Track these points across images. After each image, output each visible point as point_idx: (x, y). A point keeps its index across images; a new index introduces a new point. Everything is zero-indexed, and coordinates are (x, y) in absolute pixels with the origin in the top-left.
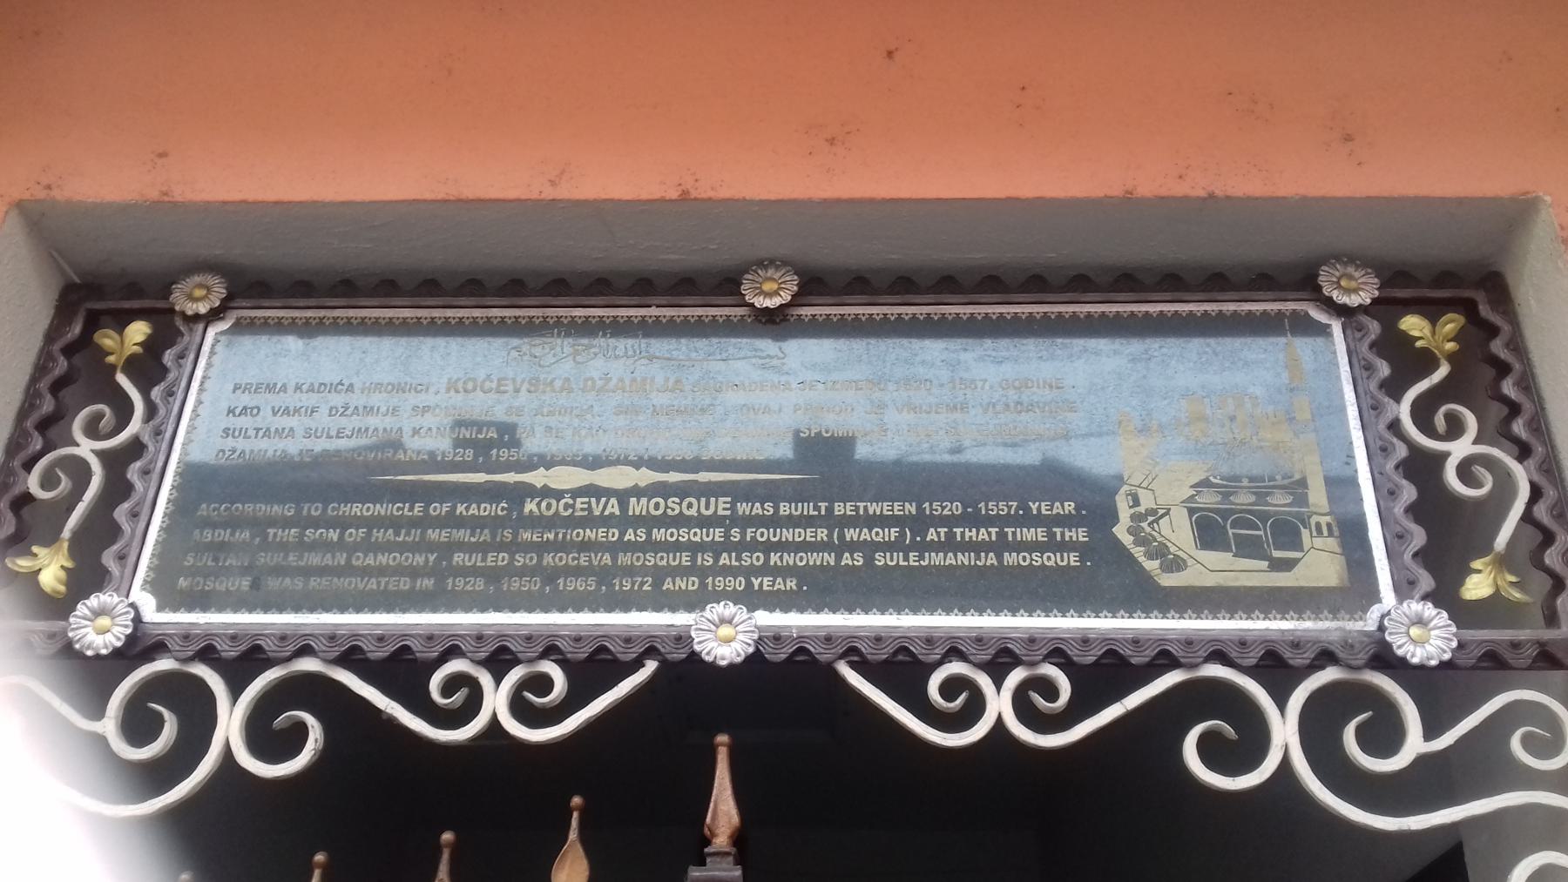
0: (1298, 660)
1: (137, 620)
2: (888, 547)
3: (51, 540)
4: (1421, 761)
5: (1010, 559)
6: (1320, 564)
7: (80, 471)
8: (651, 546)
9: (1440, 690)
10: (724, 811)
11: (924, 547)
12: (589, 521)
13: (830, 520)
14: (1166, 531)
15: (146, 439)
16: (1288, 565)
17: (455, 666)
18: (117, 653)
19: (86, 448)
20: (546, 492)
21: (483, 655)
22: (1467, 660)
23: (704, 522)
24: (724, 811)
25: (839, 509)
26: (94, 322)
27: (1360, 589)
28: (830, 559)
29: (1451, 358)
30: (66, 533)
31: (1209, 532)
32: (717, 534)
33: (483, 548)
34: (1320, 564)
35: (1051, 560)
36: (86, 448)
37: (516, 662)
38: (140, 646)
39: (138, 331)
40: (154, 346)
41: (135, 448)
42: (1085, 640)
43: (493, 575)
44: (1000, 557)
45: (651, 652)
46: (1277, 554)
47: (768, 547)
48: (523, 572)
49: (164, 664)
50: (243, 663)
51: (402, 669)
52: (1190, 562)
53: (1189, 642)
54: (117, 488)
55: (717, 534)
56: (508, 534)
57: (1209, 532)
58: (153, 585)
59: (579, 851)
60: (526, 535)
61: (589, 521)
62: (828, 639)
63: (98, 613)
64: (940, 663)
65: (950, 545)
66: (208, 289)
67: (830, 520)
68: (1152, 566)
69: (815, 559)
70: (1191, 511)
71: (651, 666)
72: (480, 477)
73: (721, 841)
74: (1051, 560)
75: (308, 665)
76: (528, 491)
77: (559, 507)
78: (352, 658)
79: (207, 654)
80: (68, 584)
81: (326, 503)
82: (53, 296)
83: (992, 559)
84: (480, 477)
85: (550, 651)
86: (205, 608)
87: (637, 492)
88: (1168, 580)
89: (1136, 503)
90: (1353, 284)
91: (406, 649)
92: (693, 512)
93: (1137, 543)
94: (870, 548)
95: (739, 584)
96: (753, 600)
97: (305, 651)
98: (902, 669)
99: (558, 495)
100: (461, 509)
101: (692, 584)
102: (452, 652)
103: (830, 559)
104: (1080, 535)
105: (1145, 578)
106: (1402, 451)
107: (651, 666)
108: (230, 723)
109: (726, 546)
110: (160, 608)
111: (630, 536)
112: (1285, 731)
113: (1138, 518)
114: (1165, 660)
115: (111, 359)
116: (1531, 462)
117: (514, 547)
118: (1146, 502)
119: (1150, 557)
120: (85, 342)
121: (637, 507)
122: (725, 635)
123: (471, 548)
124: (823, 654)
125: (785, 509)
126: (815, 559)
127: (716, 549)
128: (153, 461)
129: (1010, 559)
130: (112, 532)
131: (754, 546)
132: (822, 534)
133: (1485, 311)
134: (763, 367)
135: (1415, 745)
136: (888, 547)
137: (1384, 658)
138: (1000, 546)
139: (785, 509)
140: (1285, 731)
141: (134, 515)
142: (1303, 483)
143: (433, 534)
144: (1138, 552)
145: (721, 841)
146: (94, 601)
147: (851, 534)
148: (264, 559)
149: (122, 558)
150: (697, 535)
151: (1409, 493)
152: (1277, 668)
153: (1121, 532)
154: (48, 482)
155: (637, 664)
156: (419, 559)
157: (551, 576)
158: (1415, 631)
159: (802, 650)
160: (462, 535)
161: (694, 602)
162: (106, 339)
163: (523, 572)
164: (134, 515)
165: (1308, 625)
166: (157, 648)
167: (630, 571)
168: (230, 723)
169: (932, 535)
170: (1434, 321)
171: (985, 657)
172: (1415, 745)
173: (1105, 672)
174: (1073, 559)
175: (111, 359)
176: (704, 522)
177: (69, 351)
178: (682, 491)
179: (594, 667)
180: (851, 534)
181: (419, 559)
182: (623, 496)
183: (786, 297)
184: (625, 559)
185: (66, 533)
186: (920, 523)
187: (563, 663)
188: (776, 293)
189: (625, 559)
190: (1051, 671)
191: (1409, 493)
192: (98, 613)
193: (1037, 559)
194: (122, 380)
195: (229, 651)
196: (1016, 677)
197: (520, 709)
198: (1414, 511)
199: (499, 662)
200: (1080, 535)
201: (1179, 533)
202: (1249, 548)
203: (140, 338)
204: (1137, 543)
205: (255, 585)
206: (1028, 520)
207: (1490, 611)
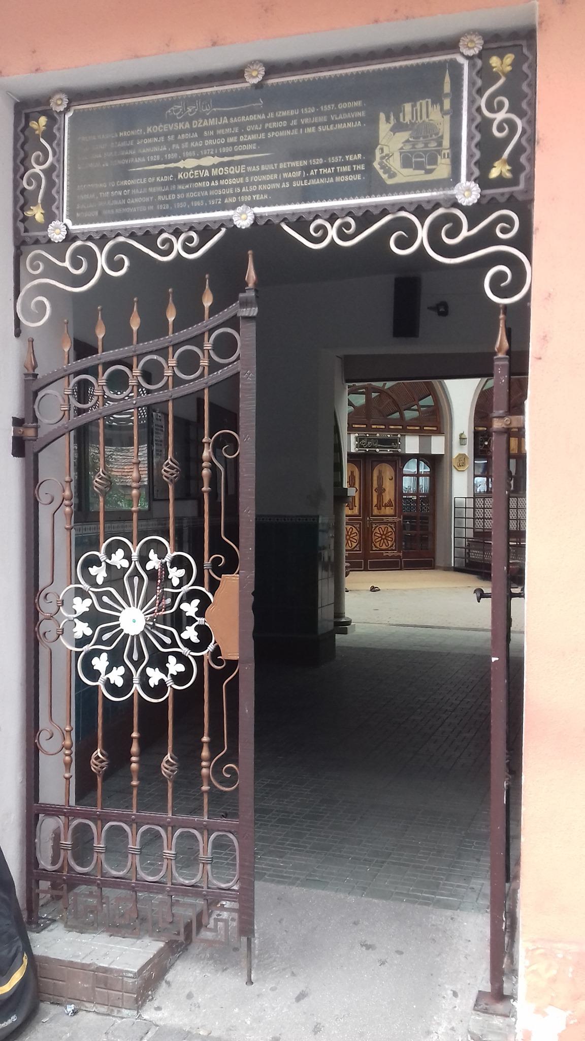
0: (428, 207)
1: (67, 229)
3: (35, 204)
4: (466, 240)
5: (338, 179)
6: (442, 170)
8: (220, 187)
9: (475, 213)
10: (251, 275)
11: (308, 178)
12: (200, 180)
13: (279, 171)
14: (391, 163)
15: (477, 97)
16: (429, 172)
17: (319, 221)
18: (64, 241)
19: (38, 169)
22: (484, 201)
23: (237, 176)
24: (251, 275)
25: (281, 165)
26: (28, 118)
27: (455, 178)
28: (278, 185)
29: (506, 75)
30: (39, 201)
32: (241, 180)
33: (167, 193)
34: (442, 170)
35: (351, 178)
36: (38, 169)
38: (70, 238)
39: (43, 120)
41: (52, 168)
42: (359, 208)
44: (334, 179)
45: (222, 225)
46: (428, 167)
47: (258, 183)
48: (180, 201)
49: (79, 243)
50: (102, 239)
51: (148, 237)
53: (393, 204)
54: (51, 184)
55: (241, 180)
56: (174, 187)
57: (406, 162)
59: (209, 292)
60: (180, 187)
61: (200, 180)
62: (277, 216)
63: (56, 228)
64: (314, 220)
65: (319, 176)
66: (62, 100)
67: (279, 171)
68: (385, 176)
69: (274, 186)
70: (401, 153)
71: (223, 230)
72: (162, 166)
73: (251, 285)
74: (351, 178)
75: (121, 239)
76: (178, 170)
77: (189, 175)
78: (132, 236)
79: (90, 238)
80: (45, 218)
81: (116, 181)
83: (332, 180)
84: (162, 166)
86: (127, 219)
87: (215, 166)
88: (389, 182)
89: (382, 152)
90: (473, 45)
91: (207, 226)
92: (233, 172)
93: (381, 168)
94: (291, 180)
95: (249, 198)
96: (252, 204)
97: (118, 235)
98: (301, 223)
99: (188, 170)
101: (234, 200)
102: (317, 217)
103: (278, 185)
104: (362, 167)
105: (382, 181)
106: (479, 119)
107: (223, 230)
108: (102, 261)
110: (73, 224)
111: (213, 184)
112: (422, 234)
113: (382, 158)
114: (384, 212)
115: (37, 132)
116: (525, 119)
117: (176, 192)
118: (386, 151)
119: (385, 173)
121: (215, 172)
122: (243, 219)
125: (263, 168)
126: (274, 186)
127: (240, 186)
128: (59, 172)
130: (53, 200)
131: (253, 183)
132: (276, 176)
133: (525, 51)
135: (465, 233)
137: (456, 205)
138: (336, 174)
139: (263, 168)
140: (422, 234)
141: (58, 192)
142: (442, 137)
143: (151, 190)
144: (381, 172)
145: (251, 285)
146: (53, 224)
147: (285, 175)
148: (101, 204)
149: (58, 208)
151: (478, 137)
152: (421, 211)
153: (376, 165)
154: (29, 184)
155: (219, 230)
156: (147, 199)
157: (189, 201)
158: (466, 194)
159: (367, 211)
161: (234, 207)
163: (180, 201)
164: (58, 192)
165: (435, 194)
167: (214, 197)
168: (102, 261)
169: (312, 173)
170: (502, 57)
171: (412, 209)
172: (465, 233)
173: (366, 218)
174: (359, 177)
175: (37, 132)
176: (237, 176)
177: (23, 131)
178: (229, 164)
179: (206, 232)
180: (285, 175)
181: (147, 199)
182: (209, 168)
183: (260, 78)
184: (212, 193)
185: (39, 201)
186: (307, 169)
187: (354, 218)
188: (257, 76)
189: (212, 193)
190: (350, 220)
191: (478, 137)
192: (56, 228)
193: (347, 178)
195: (140, 233)
196: (338, 223)
197: (342, 236)
198: (477, 145)
199: (177, 233)
200: (362, 167)
201: (395, 163)
202: (419, 166)
203: (44, 124)
204: (381, 168)
205: (100, 213)
206: (346, 163)
207: (501, 181)
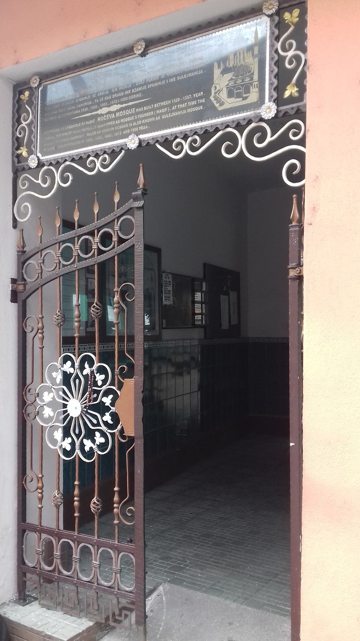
2: (164, 113)
7: (23, 129)
8: (121, 124)
11: (171, 112)
12: (110, 120)
20: (102, 115)
21: (234, 126)
23: (130, 115)
31: (230, 94)
34: (253, 96)
35: (197, 109)
37: (100, 156)
39: (27, 93)
40: (31, 96)
43: (93, 137)
49: (46, 168)
51: (81, 160)
52: (225, 102)
54: (31, 132)
58: (40, 152)
61: (110, 120)
65: (178, 110)
67: (154, 110)
70: (227, 88)
71: (123, 151)
75: (68, 163)
76: (98, 115)
78: (73, 160)
79: (51, 164)
82: (12, 89)
85: (196, 133)
97: (228, 126)
98: (167, 143)
100: (113, 129)
102: (176, 137)
103: (154, 119)
104: (203, 101)
109: (135, 120)
112: (242, 142)
113: (215, 93)
114: (217, 130)
117: (97, 130)
120: (19, 99)
121: (118, 114)
122: (132, 143)
123: (89, 132)
124: (152, 142)
127: (132, 122)
129: (189, 110)
134: (140, 71)
135: (269, 139)
136: (164, 113)
137: (262, 120)
149: (34, 147)
150: (129, 119)
153: (212, 98)
155: (120, 151)
160: (88, 129)
162: (22, 97)
165: (248, 113)
166: (43, 165)
169: (173, 108)
170: (291, 13)
172: (269, 139)
173: (206, 135)
176: (130, 115)
179: (113, 153)
194: (26, 106)
200: (203, 101)
202: (239, 95)
